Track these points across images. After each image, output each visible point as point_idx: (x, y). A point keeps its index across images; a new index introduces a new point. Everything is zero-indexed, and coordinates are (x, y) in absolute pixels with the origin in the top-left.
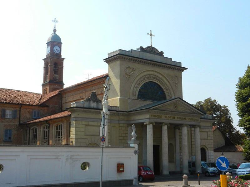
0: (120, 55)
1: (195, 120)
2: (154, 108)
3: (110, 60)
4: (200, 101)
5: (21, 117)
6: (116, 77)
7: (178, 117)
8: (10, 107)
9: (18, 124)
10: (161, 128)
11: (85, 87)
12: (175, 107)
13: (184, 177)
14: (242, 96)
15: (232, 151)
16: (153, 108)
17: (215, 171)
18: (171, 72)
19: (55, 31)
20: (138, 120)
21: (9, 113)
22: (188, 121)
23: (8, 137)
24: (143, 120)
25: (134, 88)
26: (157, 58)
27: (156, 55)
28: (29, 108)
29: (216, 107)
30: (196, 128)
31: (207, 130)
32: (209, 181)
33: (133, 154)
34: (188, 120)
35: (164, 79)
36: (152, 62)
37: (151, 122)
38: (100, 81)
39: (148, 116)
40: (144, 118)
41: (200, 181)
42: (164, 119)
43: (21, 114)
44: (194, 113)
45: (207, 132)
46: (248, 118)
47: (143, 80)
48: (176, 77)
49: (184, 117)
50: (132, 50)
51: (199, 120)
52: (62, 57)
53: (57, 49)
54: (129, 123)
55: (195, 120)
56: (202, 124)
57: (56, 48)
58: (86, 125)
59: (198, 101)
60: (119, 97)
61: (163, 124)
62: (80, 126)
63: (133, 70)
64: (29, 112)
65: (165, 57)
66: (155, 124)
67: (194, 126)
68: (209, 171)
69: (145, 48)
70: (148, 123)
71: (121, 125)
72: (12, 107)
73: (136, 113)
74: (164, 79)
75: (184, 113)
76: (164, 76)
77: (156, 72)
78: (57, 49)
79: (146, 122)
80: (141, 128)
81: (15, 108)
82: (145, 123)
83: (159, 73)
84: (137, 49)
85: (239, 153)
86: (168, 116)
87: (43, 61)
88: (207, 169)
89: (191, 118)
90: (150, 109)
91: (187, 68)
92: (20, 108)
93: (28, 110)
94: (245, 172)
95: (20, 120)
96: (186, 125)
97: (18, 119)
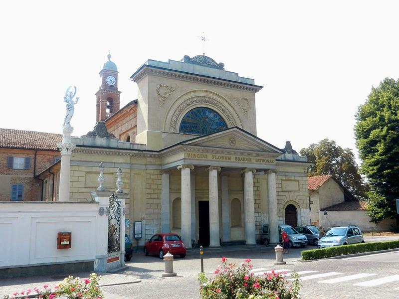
0: (148, 68)
1: (267, 161)
2: (191, 142)
3: (136, 77)
4: (313, 144)
5: (37, 168)
6: (146, 104)
7: (236, 158)
8: (21, 154)
9: (33, 176)
10: (207, 176)
11: (116, 120)
12: (230, 142)
13: (276, 249)
14: (363, 130)
15: (352, 209)
16: (188, 143)
17: (301, 240)
18: (237, 94)
19: (109, 57)
20: (171, 163)
21: (19, 162)
22: (255, 163)
23: (17, 195)
24: (175, 163)
25: (173, 117)
26: (214, 73)
27: (210, 69)
28: (49, 155)
29: (335, 150)
30: (268, 173)
31: (297, 178)
32: (261, 259)
33: (97, 214)
34: (254, 161)
35: (226, 104)
36: (202, 78)
37: (188, 165)
38: (128, 110)
39: (182, 156)
40: (176, 160)
41: (204, 259)
42: (211, 161)
43: (36, 162)
44: (265, 151)
45: (298, 181)
46: (370, 161)
47: (190, 105)
48: (246, 100)
49: (247, 157)
50: (169, 60)
51: (275, 162)
52: (119, 90)
53: (111, 80)
54: (163, 168)
55: (267, 161)
56: (279, 169)
57: (110, 79)
58: (87, 173)
59: (312, 144)
60: (147, 130)
61: (210, 168)
62: (76, 174)
63: (172, 89)
64: (49, 160)
65: (226, 71)
66: (193, 168)
67: (266, 171)
68: (292, 240)
69: (193, 58)
70: (181, 167)
71: (149, 171)
72: (23, 154)
73: (169, 152)
74: (226, 104)
75: (247, 150)
76: (225, 99)
77: (211, 93)
78: (111, 80)
79: (180, 164)
80: (174, 174)
81: (28, 154)
82: (178, 168)
83: (216, 94)
84: (182, 60)
85: (364, 213)
86: (217, 155)
87: (96, 96)
88: (289, 237)
89: (259, 158)
90: (184, 144)
91: (263, 87)
92: (35, 155)
93: (48, 157)
94: (331, 242)
95: (35, 170)
96: (251, 170)
97: (33, 170)
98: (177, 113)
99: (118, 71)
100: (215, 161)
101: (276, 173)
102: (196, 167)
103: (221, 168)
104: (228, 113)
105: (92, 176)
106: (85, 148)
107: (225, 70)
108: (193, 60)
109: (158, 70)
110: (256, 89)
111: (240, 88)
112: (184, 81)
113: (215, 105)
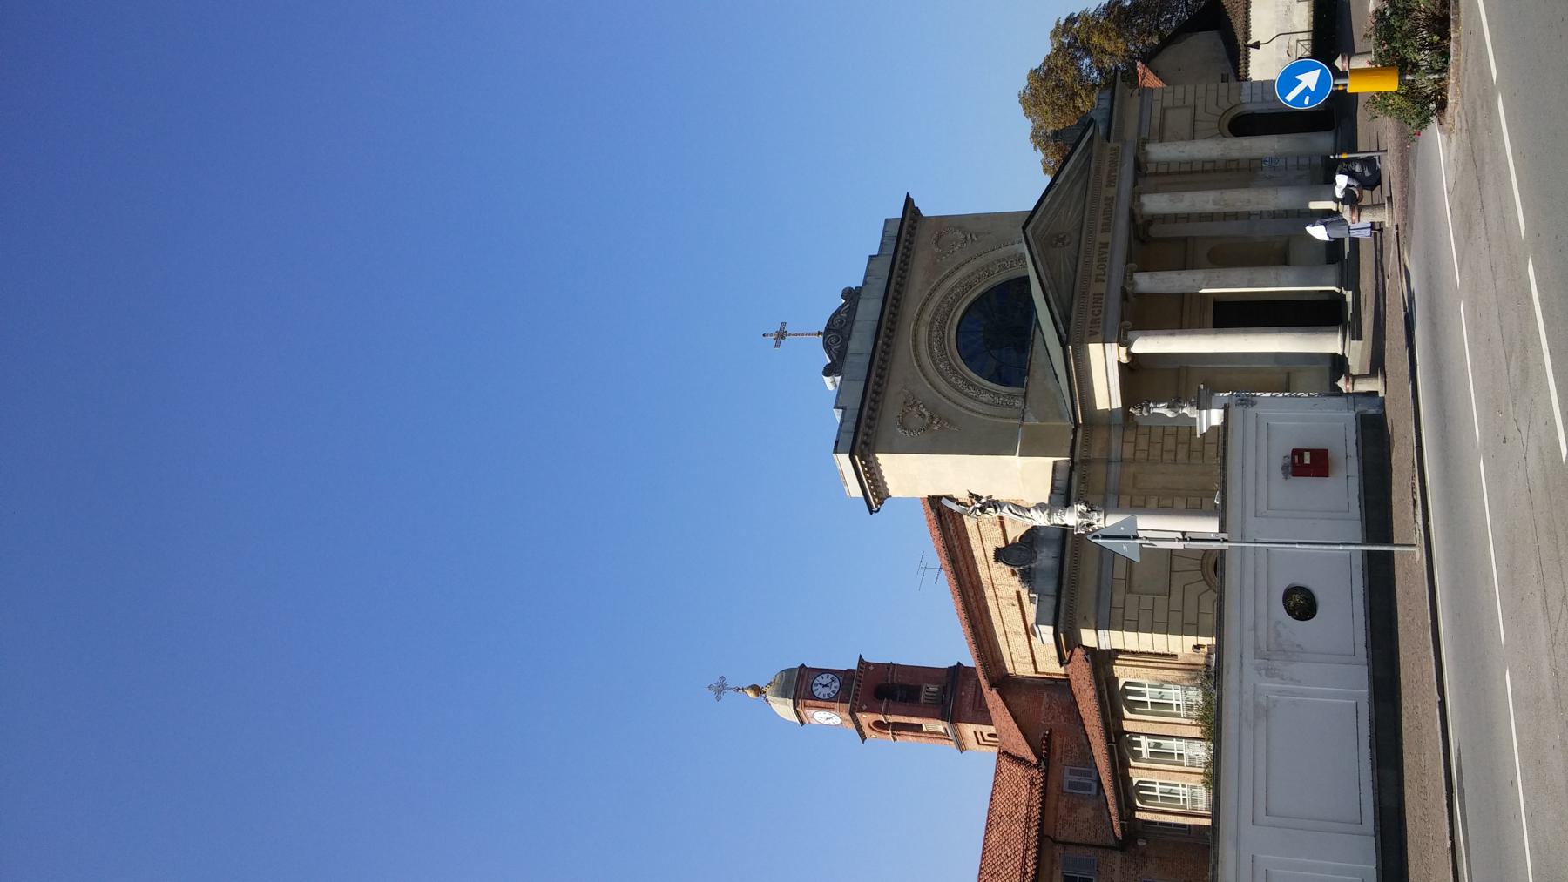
9: (1118, 855)
26: (869, 311)
28: (1056, 808)
34: (1112, 192)
35: (950, 283)
36: (882, 334)
42: (1108, 285)
45: (1164, 110)
47: (950, 364)
58: (1129, 589)
61: (1129, 289)
65: (865, 282)
67: (1139, 167)
72: (1052, 873)
75: (1084, 205)
76: (938, 285)
82: (1124, 360)
91: (908, 195)
93: (1062, 811)
96: (1136, 196)
98: (971, 391)
99: (797, 665)
100: (1109, 277)
101: (1145, 141)
102: (1129, 259)
103: (1122, 320)
104: (973, 278)
105: (1136, 577)
106: (1065, 587)
107: (861, 285)
108: (835, 358)
109: (862, 427)
110: (913, 212)
111: (908, 249)
112: (889, 374)
113: (952, 307)
